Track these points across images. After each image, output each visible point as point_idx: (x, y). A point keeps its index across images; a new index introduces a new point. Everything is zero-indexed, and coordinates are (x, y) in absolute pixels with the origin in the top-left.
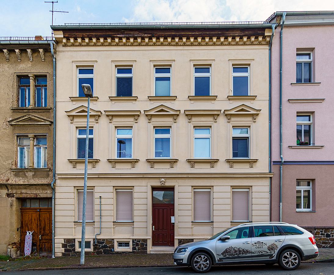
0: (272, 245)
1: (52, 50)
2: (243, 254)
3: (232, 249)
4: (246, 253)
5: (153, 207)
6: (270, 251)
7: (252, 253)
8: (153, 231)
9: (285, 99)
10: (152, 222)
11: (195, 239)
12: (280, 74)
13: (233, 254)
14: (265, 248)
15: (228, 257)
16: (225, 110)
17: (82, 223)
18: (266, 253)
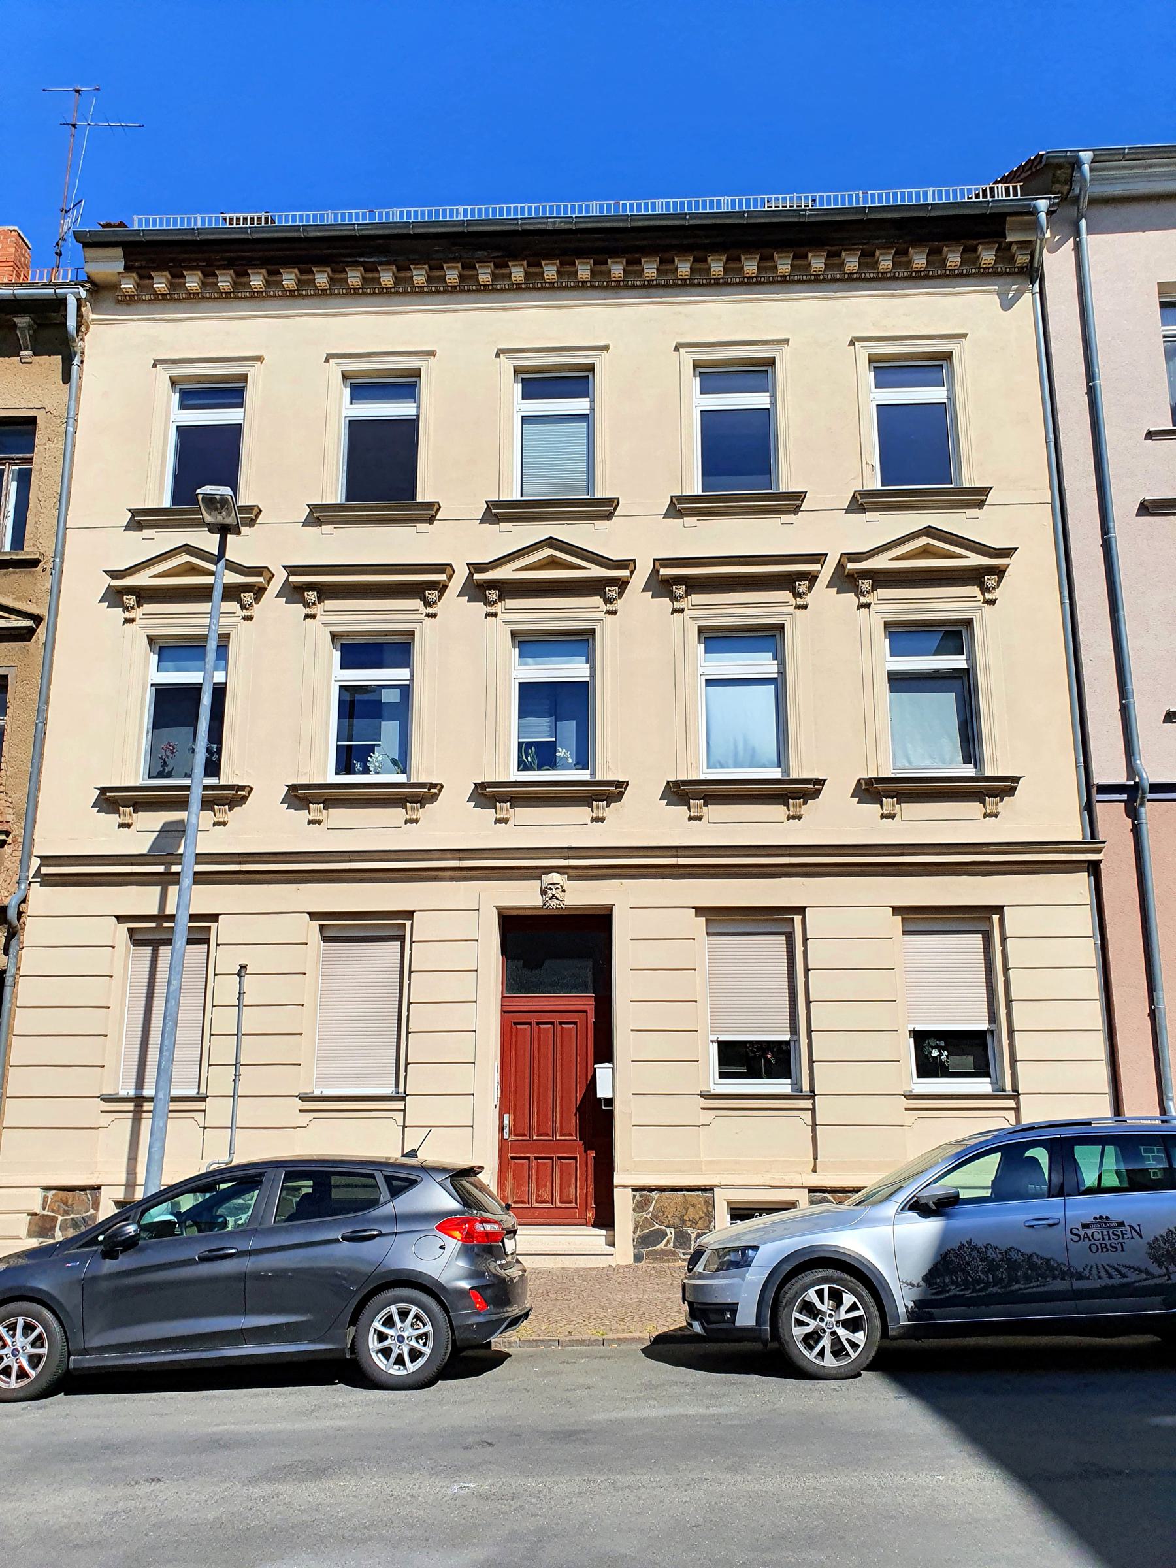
0: (1167, 1234)
1: (72, 322)
2: (1028, 1279)
3: (974, 1254)
4: (1044, 1277)
5: (504, 1012)
6: (1160, 1266)
7: (1072, 1276)
8: (503, 1141)
9: (1123, 505)
10: (497, 1093)
11: (719, 1187)
12: (1092, 393)
13: (980, 1281)
14: (1136, 1254)
15: (955, 1296)
16: (842, 554)
17: (170, 1108)
18: (1144, 1276)
